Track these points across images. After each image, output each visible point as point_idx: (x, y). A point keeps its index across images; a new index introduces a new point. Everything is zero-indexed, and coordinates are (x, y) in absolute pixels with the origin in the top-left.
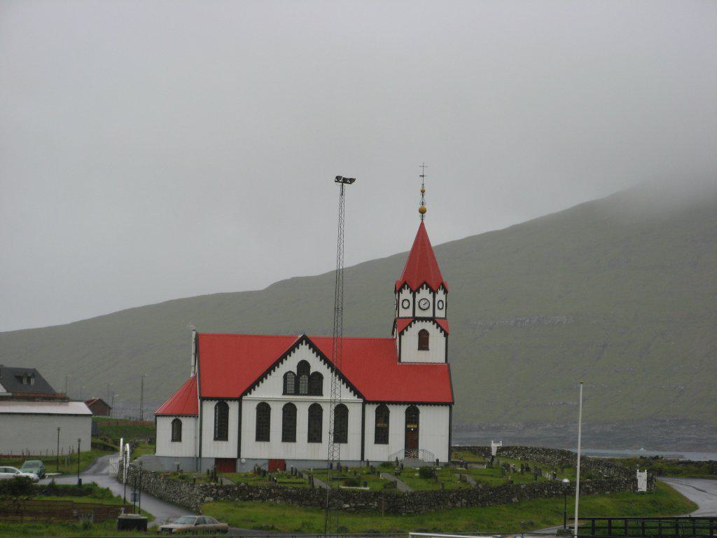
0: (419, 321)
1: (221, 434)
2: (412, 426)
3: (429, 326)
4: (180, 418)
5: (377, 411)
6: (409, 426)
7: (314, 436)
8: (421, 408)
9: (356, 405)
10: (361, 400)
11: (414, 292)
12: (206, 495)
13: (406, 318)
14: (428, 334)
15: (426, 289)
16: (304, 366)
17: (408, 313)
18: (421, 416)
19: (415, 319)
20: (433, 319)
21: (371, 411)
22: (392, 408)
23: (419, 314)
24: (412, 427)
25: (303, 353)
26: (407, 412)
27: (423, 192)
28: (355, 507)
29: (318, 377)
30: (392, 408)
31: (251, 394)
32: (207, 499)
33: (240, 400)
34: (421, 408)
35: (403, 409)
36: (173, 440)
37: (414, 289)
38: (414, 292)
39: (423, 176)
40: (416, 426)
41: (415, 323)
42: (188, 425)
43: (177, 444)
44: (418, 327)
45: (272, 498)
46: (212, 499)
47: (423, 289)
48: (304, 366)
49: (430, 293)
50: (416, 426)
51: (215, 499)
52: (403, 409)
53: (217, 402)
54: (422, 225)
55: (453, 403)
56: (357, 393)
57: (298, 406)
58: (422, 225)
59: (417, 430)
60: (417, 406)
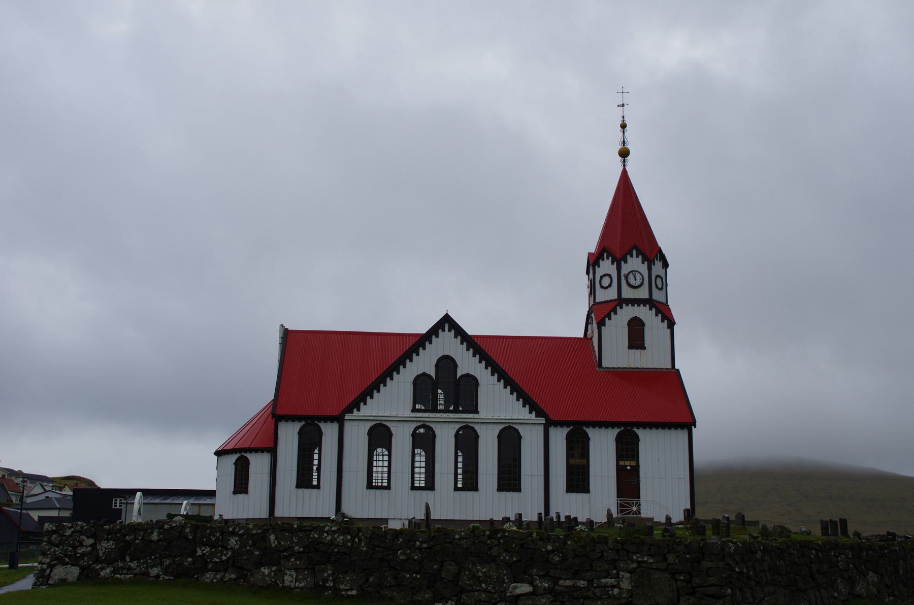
0: (627, 305)
1: (305, 480)
2: (627, 463)
3: (645, 314)
4: (249, 456)
5: (569, 438)
6: (622, 463)
7: (470, 483)
8: (641, 433)
9: (534, 428)
10: (542, 420)
11: (619, 261)
12: (60, 560)
13: (606, 302)
14: (643, 324)
15: (637, 256)
16: (446, 363)
17: (612, 294)
18: (641, 445)
19: (621, 301)
20: (649, 302)
21: (559, 437)
22: (592, 433)
23: (627, 293)
24: (628, 464)
25: (447, 344)
26: (619, 439)
27: (623, 126)
28: (550, 591)
29: (472, 382)
30: (592, 433)
31: (359, 410)
32: (59, 572)
33: (339, 420)
34: (641, 433)
35: (612, 433)
36: (236, 492)
37: (618, 256)
38: (619, 261)
39: (623, 105)
40: (633, 463)
41: (621, 308)
42: (259, 464)
43: (241, 497)
44: (626, 313)
45: (269, 565)
46: (75, 571)
47: (632, 256)
48: (446, 363)
49: (643, 263)
50: (633, 463)
51: (88, 576)
52: (612, 433)
53: (303, 423)
54: (625, 172)
55: (694, 424)
56: (534, 408)
57: (437, 429)
58: (625, 172)
59: (636, 470)
60: (635, 430)
